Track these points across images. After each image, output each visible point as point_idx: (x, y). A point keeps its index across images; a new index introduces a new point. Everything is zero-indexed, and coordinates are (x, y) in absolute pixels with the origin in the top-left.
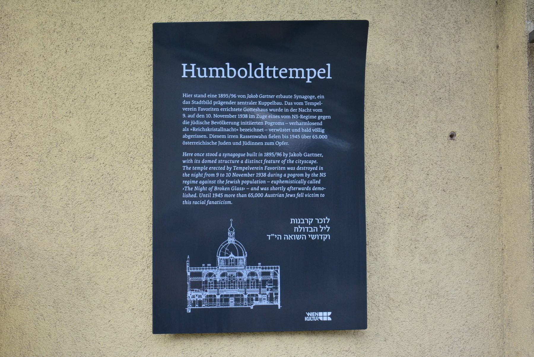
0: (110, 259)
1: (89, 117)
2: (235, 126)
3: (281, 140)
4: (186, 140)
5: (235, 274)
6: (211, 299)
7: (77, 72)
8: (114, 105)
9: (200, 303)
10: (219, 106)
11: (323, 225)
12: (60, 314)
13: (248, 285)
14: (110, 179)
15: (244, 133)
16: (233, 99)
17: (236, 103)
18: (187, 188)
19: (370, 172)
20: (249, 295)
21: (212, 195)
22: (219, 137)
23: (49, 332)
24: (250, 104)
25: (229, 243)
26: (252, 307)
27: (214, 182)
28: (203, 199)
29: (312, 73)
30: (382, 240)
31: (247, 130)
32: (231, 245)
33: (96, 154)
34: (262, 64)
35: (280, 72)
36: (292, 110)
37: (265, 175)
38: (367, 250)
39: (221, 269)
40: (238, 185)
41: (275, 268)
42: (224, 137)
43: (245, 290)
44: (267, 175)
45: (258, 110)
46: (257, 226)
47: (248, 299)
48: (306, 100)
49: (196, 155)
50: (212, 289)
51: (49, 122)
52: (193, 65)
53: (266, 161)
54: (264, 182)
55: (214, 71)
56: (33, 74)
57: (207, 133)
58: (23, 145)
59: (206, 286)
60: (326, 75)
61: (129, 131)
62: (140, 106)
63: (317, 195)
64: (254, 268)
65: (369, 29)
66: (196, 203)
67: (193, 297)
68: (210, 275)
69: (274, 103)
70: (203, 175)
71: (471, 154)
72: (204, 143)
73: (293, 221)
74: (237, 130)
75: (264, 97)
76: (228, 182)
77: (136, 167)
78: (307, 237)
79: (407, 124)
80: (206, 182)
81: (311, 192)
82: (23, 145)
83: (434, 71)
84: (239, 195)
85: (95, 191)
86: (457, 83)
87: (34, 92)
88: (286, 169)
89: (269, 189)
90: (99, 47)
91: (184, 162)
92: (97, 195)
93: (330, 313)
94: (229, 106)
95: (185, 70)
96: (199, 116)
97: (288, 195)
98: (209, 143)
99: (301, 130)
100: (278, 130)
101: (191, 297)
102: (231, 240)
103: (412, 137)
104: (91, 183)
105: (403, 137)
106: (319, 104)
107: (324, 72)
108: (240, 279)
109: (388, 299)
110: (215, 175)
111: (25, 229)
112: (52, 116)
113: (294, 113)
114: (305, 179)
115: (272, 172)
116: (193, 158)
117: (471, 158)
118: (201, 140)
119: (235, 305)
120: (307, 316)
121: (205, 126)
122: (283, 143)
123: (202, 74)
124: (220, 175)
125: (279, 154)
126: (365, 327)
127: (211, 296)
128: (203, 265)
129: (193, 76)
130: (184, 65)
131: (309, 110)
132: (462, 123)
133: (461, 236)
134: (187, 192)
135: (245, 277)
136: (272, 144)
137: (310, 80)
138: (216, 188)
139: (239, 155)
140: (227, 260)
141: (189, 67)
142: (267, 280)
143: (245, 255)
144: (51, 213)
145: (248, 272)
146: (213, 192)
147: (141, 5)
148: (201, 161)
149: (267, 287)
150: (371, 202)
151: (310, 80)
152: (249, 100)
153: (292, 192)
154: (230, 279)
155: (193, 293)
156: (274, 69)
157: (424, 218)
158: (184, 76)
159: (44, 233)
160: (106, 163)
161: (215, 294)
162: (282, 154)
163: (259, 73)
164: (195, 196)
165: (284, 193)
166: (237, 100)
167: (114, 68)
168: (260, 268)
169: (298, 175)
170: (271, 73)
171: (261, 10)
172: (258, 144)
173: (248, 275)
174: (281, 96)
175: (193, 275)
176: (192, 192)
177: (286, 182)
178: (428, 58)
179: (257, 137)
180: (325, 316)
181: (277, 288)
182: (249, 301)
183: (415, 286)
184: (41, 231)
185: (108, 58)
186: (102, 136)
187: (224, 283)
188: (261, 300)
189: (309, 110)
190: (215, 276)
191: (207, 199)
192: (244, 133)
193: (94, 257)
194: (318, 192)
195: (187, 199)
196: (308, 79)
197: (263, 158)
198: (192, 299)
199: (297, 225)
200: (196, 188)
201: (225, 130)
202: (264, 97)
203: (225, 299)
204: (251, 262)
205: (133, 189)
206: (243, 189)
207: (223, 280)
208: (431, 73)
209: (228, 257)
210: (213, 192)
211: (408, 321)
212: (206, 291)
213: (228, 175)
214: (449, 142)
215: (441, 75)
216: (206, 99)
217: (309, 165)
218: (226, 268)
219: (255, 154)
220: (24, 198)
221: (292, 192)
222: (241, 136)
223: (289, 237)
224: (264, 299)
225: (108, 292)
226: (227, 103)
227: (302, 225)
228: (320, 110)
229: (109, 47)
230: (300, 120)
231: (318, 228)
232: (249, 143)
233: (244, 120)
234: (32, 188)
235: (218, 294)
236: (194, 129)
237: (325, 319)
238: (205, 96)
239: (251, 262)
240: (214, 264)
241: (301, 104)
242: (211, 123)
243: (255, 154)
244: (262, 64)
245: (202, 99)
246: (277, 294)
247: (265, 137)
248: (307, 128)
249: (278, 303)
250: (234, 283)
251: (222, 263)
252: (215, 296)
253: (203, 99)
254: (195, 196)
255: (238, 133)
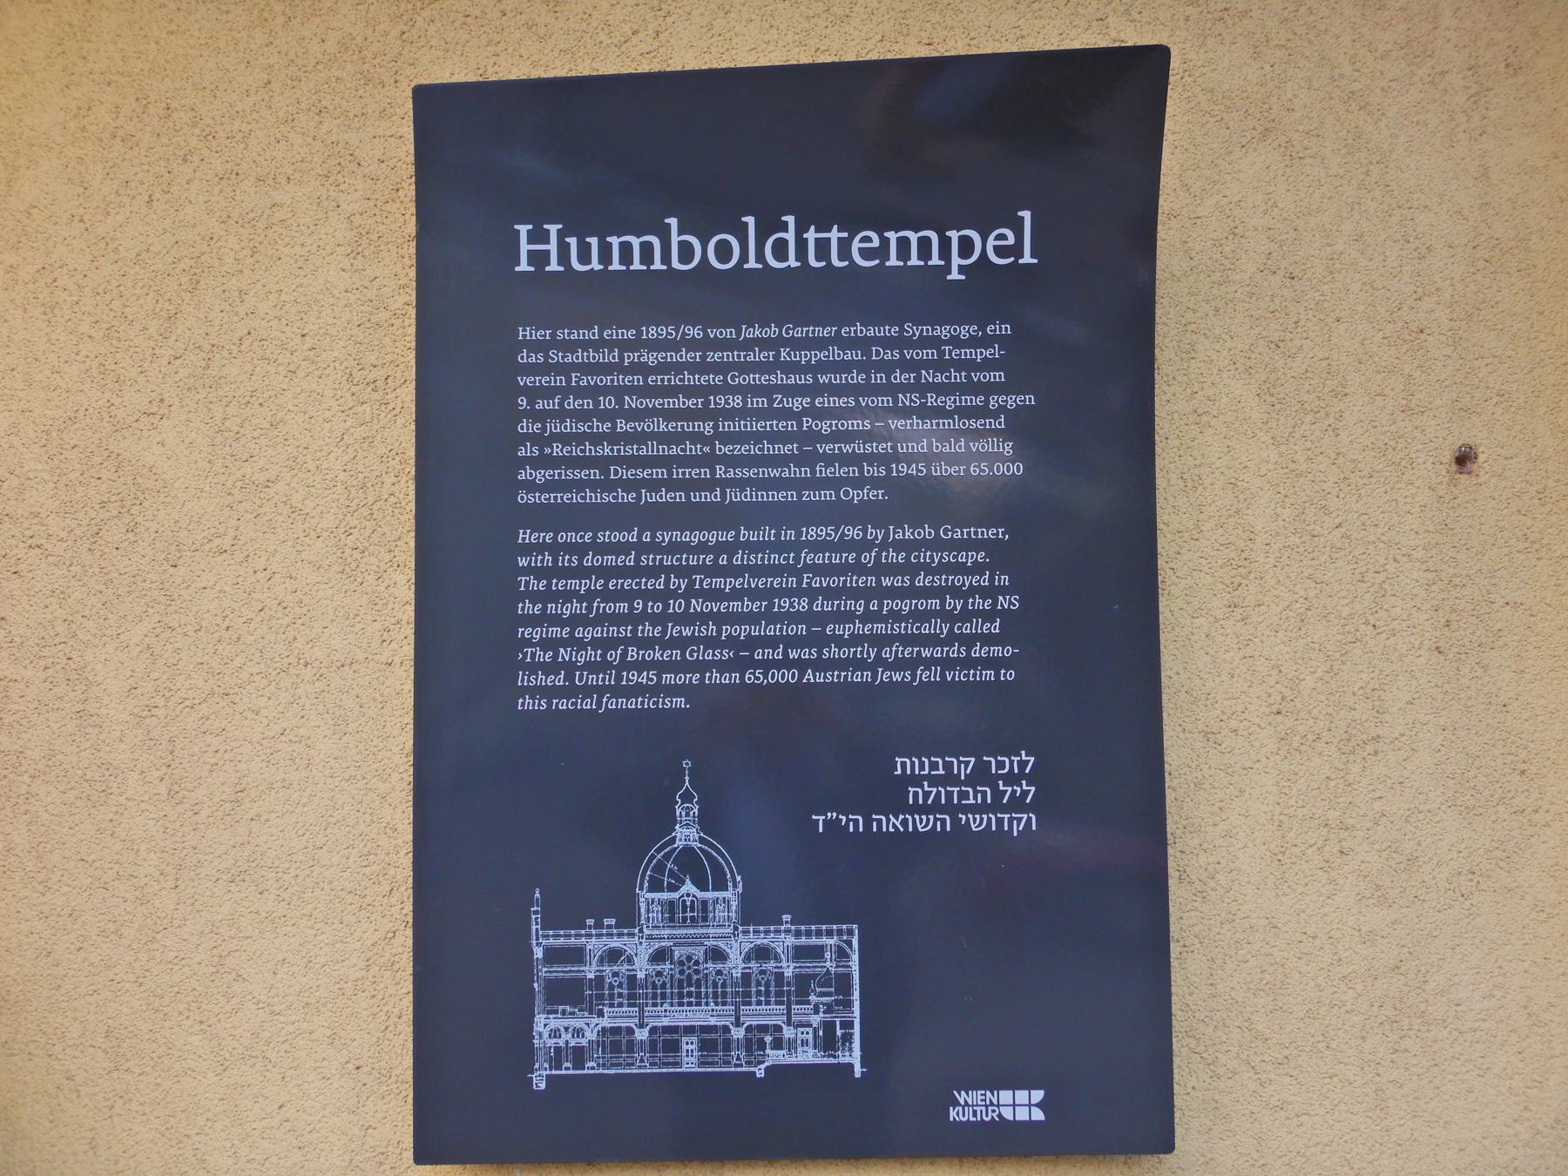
0: (285, 895)
1: (219, 417)
2: (697, 438)
3: (859, 483)
4: (531, 486)
5: (699, 953)
6: (616, 1041)
7: (181, 266)
8: (301, 374)
9: (579, 1056)
10: (644, 369)
11: (1011, 779)
12: (127, 1077)
13: (747, 994)
14: (287, 620)
15: (732, 461)
16: (692, 345)
17: (703, 357)
18: (533, 654)
19: (1176, 591)
20: (749, 1029)
21: (619, 678)
22: (643, 474)
23: (90, 1134)
24: (751, 358)
25: (679, 844)
26: (760, 1072)
27: (626, 631)
28: (588, 691)
29: (966, 247)
30: (1223, 826)
31: (741, 449)
32: (687, 850)
33: (243, 539)
34: (790, 220)
35: (856, 245)
36: (899, 377)
37: (802, 605)
38: (1171, 863)
39: (650, 937)
40: (712, 643)
41: (840, 932)
42: (660, 473)
43: (737, 1010)
44: (810, 604)
45: (779, 378)
46: (784, 774)
47: (748, 1041)
48: (946, 343)
49: (563, 537)
50: (620, 1005)
51: (98, 435)
52: (553, 229)
53: (807, 557)
54: (802, 629)
55: (626, 249)
56: (49, 280)
57: (603, 463)
58: (20, 512)
59: (600, 997)
60: (1017, 250)
61: (346, 458)
62: (382, 373)
63: (989, 674)
64: (767, 932)
65: (1170, 92)
66: (564, 705)
67: (555, 1033)
68: (613, 956)
69: (834, 353)
70: (589, 609)
71: (1529, 523)
72: (591, 497)
73: (904, 765)
74: (707, 449)
75: (799, 333)
76: (673, 631)
77: (371, 579)
78: (955, 821)
79: (1308, 419)
80: (598, 633)
81: (968, 663)
82: (20, 512)
83: (1398, 236)
84: (714, 677)
85: (238, 661)
86: (1479, 277)
87: (53, 337)
88: (879, 582)
89: (820, 653)
90: (252, 179)
91: (523, 562)
92: (245, 675)
93: (1038, 1095)
94: (678, 368)
95: (525, 247)
96: (572, 403)
97: (884, 676)
98: (608, 498)
99: (930, 445)
100: (847, 449)
101: (546, 1035)
102: (686, 835)
103: (1322, 467)
104: (226, 635)
105: (1292, 466)
106: (994, 352)
107: (1011, 240)
108: (719, 973)
109: (1247, 1034)
110: (631, 608)
111: (24, 789)
112: (106, 415)
113: (905, 388)
114: (947, 616)
115: (830, 594)
116: (555, 548)
117: (1532, 537)
118: (580, 485)
119: (701, 1064)
120: (957, 1103)
121: (596, 439)
122: (868, 494)
123: (584, 257)
124: (645, 606)
125: (853, 533)
126: (1167, 1146)
127: (616, 1031)
128: (590, 922)
129: (554, 266)
130: (523, 229)
131: (958, 377)
132: (1497, 416)
133: (1501, 809)
134: (534, 668)
135: (736, 965)
136: (828, 495)
137: (961, 269)
138: (633, 653)
139: (713, 537)
140: (671, 903)
141: (539, 236)
142: (814, 976)
143: (735, 886)
144: (102, 737)
145: (747, 947)
146: (625, 665)
147: (386, 34)
148: (580, 561)
149: (813, 998)
150: (1182, 695)
151: (961, 269)
152: (748, 345)
153: (899, 664)
154: (682, 972)
155: (555, 1023)
156: (834, 235)
157: (1369, 749)
158: (524, 266)
159: (79, 803)
160: (274, 567)
161: (632, 1023)
162: (865, 531)
163: (780, 250)
164: (560, 680)
165: (873, 668)
166: (706, 344)
167: (298, 249)
168: (787, 931)
169: (922, 604)
170: (823, 247)
171: (790, 37)
172: (779, 496)
173: (747, 959)
174: (859, 330)
175: (553, 955)
176: (551, 668)
177: (880, 628)
178: (1377, 193)
179: (775, 473)
180: (1022, 1105)
181: (848, 1004)
182: (749, 1049)
183: (1343, 987)
184: (71, 794)
185: (280, 215)
186: (261, 478)
187: (663, 986)
188: (792, 1046)
189: (958, 377)
190: (630, 960)
191: (601, 690)
192: (732, 461)
193: (233, 887)
194: (993, 661)
195: (534, 692)
196: (955, 269)
197: (797, 546)
198: (551, 1042)
199: (917, 780)
200: (564, 654)
201: (663, 450)
202: (799, 333)
203: (667, 1042)
204: (754, 913)
205: (360, 656)
206: (727, 654)
207: (659, 974)
208: (1389, 243)
209: (675, 895)
210: (625, 665)
211: (1322, 1111)
212: (601, 1014)
213: (676, 606)
214: (1452, 482)
215: (1423, 251)
216: (598, 345)
217: (960, 569)
218: (667, 932)
219: (768, 534)
220: (22, 686)
221: (899, 664)
222: (720, 471)
223: (891, 823)
224: (805, 1043)
225: (276, 1009)
226: (673, 357)
227: (935, 781)
228: (998, 376)
229: (284, 181)
230: (925, 412)
231: (995, 789)
232: (748, 496)
233: (730, 414)
234: (46, 652)
235: (641, 1026)
236: (557, 450)
237: (1022, 1115)
238: (593, 334)
239: (754, 913)
240: (628, 919)
241: (929, 354)
242: (614, 426)
243: (768, 534)
244: (790, 220)
245: (585, 345)
246: (848, 1025)
247: (805, 472)
248: (968, 451)
249: (853, 1057)
250: (698, 985)
251: (657, 913)
252: (630, 1031)
253: (588, 342)
254: (560, 680)
255: (710, 460)
